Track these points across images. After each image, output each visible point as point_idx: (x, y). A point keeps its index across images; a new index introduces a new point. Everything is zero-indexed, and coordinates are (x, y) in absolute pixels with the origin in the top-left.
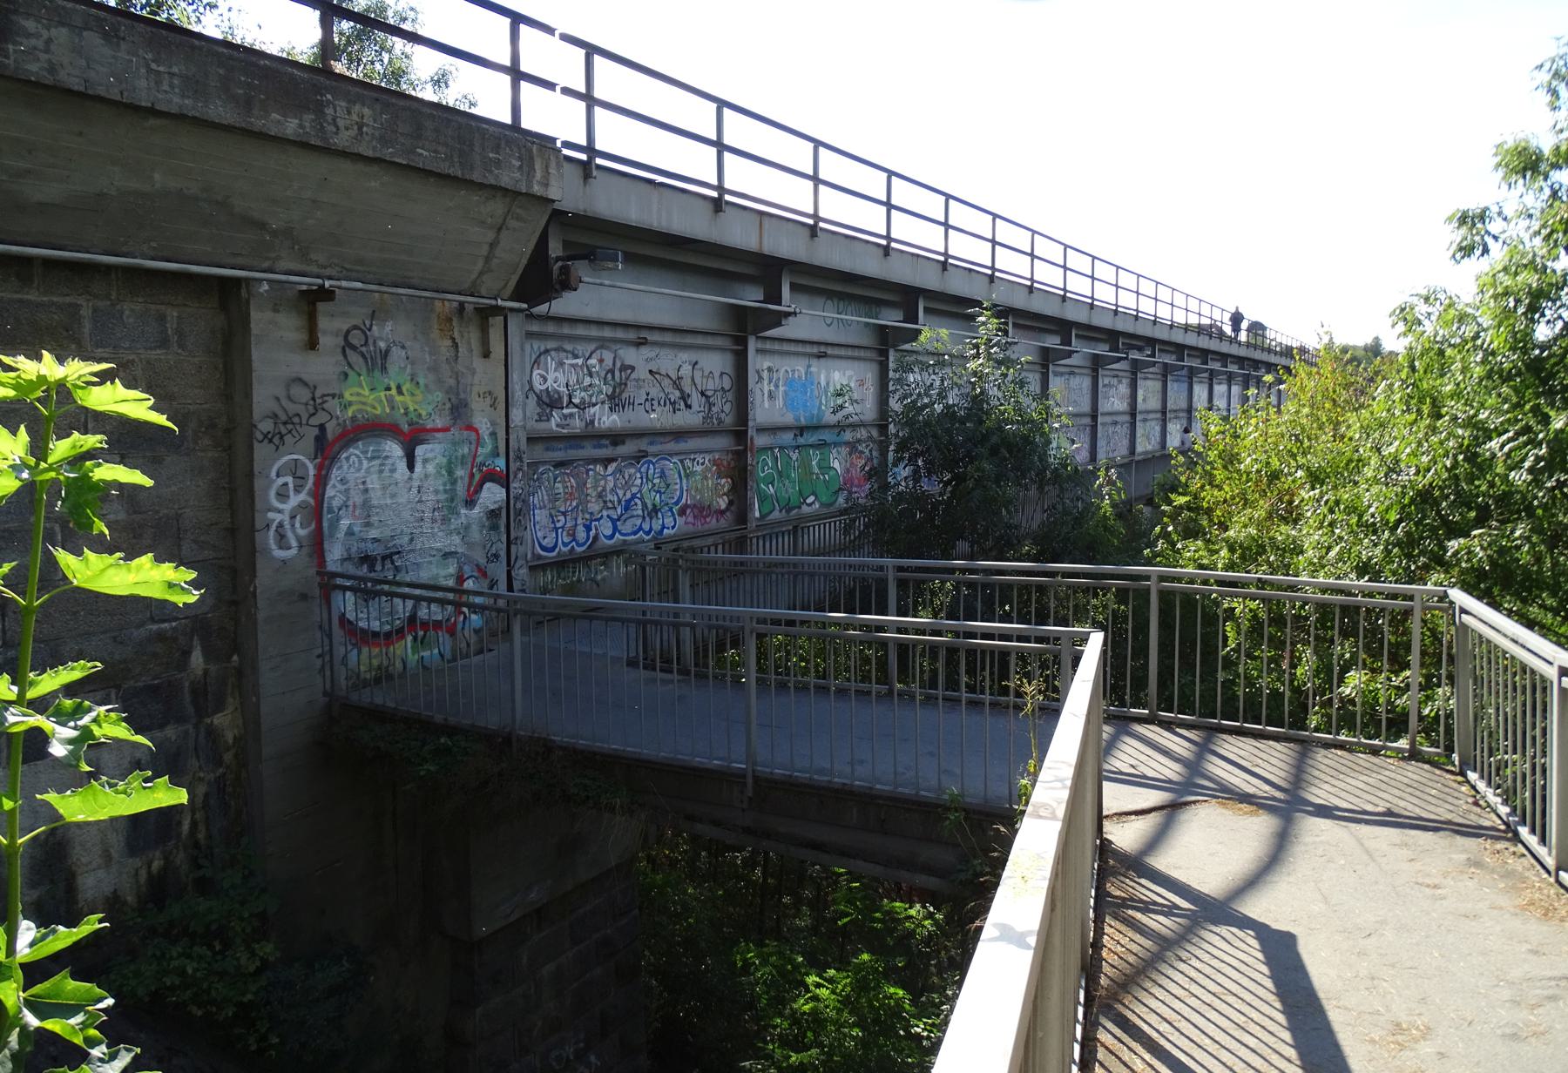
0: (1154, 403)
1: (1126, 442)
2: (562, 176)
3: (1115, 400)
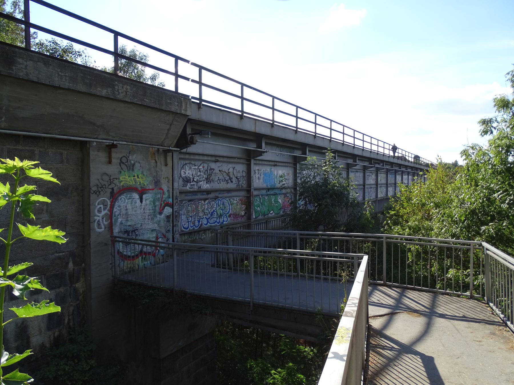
1: (374, 194)
3: (371, 180)
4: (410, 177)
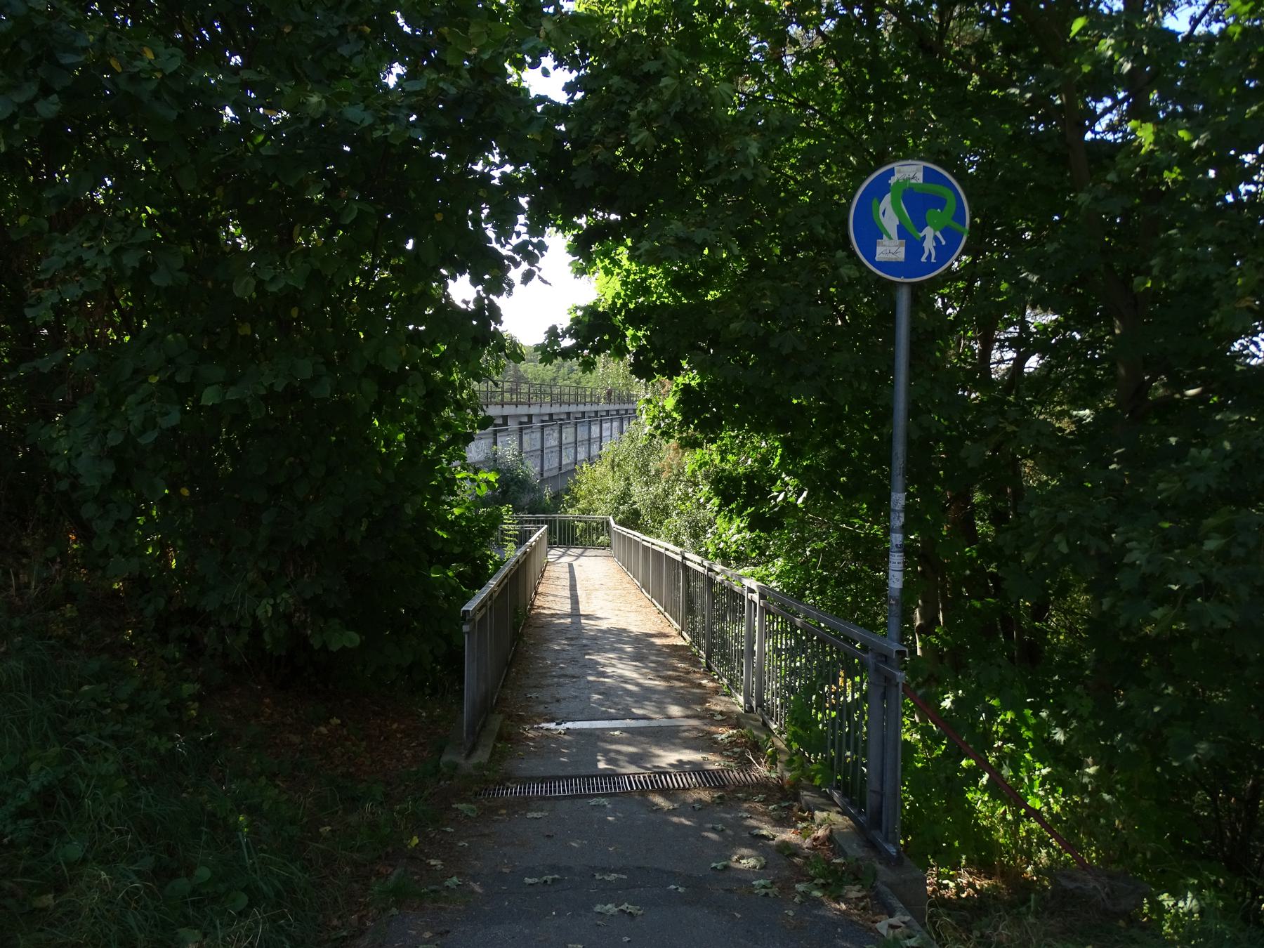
0: (571, 439)
1: (557, 460)
2: (1083, 203)
3: (552, 441)
4: (615, 424)
